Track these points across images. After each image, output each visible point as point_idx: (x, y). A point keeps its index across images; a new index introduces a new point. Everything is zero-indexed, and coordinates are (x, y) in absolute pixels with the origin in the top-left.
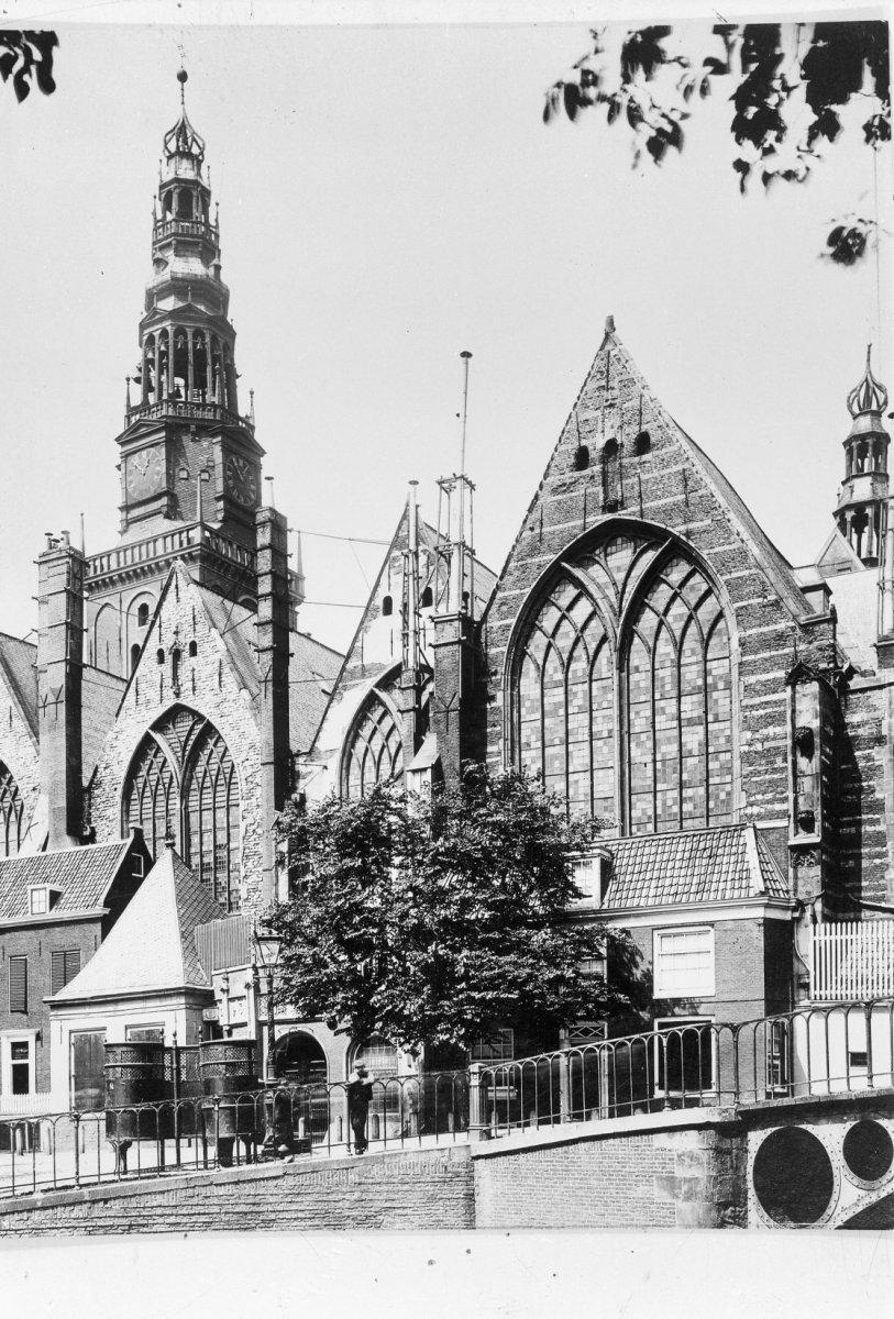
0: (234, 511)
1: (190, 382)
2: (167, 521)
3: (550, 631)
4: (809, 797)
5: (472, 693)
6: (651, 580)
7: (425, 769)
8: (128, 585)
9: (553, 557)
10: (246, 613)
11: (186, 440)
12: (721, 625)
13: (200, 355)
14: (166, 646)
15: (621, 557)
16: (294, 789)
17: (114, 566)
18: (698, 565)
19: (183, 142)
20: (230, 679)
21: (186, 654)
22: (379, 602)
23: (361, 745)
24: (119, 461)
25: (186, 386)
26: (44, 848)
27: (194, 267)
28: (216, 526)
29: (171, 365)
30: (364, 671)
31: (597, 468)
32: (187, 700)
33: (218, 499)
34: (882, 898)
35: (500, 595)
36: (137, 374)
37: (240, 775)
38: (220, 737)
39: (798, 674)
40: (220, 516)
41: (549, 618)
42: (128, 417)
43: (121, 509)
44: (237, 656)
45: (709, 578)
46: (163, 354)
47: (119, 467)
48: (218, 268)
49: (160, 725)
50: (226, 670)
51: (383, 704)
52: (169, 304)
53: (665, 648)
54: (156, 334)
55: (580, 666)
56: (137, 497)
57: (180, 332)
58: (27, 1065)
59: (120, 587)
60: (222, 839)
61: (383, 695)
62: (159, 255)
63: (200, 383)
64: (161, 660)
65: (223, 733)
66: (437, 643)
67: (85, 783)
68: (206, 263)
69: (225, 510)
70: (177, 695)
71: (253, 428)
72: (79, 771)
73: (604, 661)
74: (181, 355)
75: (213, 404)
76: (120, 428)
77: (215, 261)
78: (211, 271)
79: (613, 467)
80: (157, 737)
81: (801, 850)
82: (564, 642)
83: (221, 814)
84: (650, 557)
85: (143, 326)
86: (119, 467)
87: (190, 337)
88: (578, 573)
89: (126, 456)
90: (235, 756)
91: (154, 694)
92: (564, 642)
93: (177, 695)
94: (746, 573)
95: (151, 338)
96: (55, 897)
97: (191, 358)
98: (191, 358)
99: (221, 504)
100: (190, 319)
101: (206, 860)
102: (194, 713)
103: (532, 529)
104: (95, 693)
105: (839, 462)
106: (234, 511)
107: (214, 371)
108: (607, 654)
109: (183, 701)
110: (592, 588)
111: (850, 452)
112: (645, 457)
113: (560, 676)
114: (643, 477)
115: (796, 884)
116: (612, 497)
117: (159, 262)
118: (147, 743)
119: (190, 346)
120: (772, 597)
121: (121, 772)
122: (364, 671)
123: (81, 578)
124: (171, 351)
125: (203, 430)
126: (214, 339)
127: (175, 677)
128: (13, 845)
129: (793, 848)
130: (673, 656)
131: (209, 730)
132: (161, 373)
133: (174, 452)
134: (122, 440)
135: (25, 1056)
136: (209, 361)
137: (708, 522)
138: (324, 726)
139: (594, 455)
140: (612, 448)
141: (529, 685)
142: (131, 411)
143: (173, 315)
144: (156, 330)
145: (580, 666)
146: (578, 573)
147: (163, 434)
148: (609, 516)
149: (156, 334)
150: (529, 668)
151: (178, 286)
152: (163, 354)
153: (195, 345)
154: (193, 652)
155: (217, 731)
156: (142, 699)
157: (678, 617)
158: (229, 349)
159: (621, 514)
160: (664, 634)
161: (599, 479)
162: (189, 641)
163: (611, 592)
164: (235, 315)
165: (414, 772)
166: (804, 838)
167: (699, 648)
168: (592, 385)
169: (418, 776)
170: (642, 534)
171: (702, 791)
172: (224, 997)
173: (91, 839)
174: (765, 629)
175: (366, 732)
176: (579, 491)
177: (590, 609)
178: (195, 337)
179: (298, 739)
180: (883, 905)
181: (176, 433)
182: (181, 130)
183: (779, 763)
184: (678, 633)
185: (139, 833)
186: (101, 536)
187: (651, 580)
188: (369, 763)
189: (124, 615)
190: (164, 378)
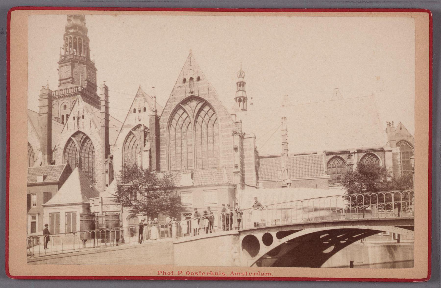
0: (89, 84)
1: (78, 50)
2: (71, 85)
3: (177, 120)
5: (155, 134)
6: (200, 110)
7: (147, 151)
8: (60, 100)
10: (97, 110)
11: (76, 64)
12: (216, 121)
13: (80, 45)
14: (76, 116)
15: (193, 104)
16: (110, 154)
18: (211, 108)
21: (81, 118)
22: (132, 110)
23: (127, 144)
24: (58, 68)
25: (76, 51)
26: (41, 165)
28: (85, 87)
29: (73, 46)
30: (127, 126)
33: (85, 80)
35: (165, 111)
36: (62, 47)
37: (96, 149)
38: (90, 140)
39: (235, 133)
40: (86, 85)
41: (177, 117)
42: (61, 57)
43: (59, 80)
45: (214, 111)
46: (70, 43)
47: (58, 70)
48: (85, 23)
49: (74, 135)
50: (92, 123)
51: (133, 134)
53: (204, 125)
54: (69, 38)
55: (184, 129)
56: (63, 78)
57: (75, 38)
58: (35, 222)
59: (58, 100)
60: (90, 165)
61: (133, 132)
62: (69, 18)
63: (80, 51)
65: (91, 139)
66: (146, 121)
67: (53, 149)
68: (82, 22)
69: (87, 83)
70: (79, 128)
71: (94, 64)
72: (51, 146)
73: (190, 128)
74: (75, 44)
75: (84, 57)
77: (84, 22)
78: (83, 24)
80: (73, 138)
82: (180, 123)
83: (90, 159)
84: (201, 104)
85: (65, 35)
86: (58, 70)
87: (78, 40)
88: (183, 106)
89: (60, 67)
90: (95, 144)
91: (72, 127)
92: (180, 123)
93: (79, 128)
95: (67, 39)
96: (45, 177)
97: (78, 45)
98: (78, 45)
99: (86, 82)
100: (78, 35)
101: (86, 170)
102: (83, 133)
104: (55, 125)
105: (235, 87)
106: (89, 84)
107: (84, 49)
108: (191, 125)
109: (80, 130)
110: (187, 111)
111: (238, 85)
112: (199, 82)
113: (180, 131)
114: (199, 86)
116: (192, 90)
118: (70, 139)
119: (78, 41)
121: (63, 147)
122: (127, 126)
123: (50, 98)
124: (73, 43)
125: (81, 62)
126: (84, 41)
127: (78, 124)
128: (31, 164)
129: (234, 172)
130: (206, 128)
131: (87, 137)
132: (70, 47)
133: (73, 67)
134: (59, 63)
135: (35, 219)
136: (83, 46)
138: (117, 139)
140: (191, 79)
141: (172, 133)
142: (62, 56)
143: (73, 33)
145: (184, 129)
146: (183, 106)
148: (191, 95)
149: (69, 38)
150: (172, 129)
151: (74, 27)
152: (70, 43)
153: (79, 42)
155: (89, 138)
156: (69, 129)
157: (207, 119)
158: (88, 44)
159: (193, 94)
160: (204, 123)
161: (188, 86)
162: (82, 115)
163: (191, 112)
164: (89, 35)
165: (144, 151)
166: (236, 170)
167: (212, 126)
169: (145, 152)
170: (199, 99)
171: (213, 159)
172: (93, 205)
173: (54, 163)
175: (129, 140)
176: (184, 88)
177: (187, 116)
178: (79, 40)
179: (111, 142)
181: (74, 62)
183: (230, 153)
184: (207, 122)
185: (68, 161)
186: (54, 87)
187: (200, 110)
188: (130, 148)
189: (60, 106)
190: (71, 49)
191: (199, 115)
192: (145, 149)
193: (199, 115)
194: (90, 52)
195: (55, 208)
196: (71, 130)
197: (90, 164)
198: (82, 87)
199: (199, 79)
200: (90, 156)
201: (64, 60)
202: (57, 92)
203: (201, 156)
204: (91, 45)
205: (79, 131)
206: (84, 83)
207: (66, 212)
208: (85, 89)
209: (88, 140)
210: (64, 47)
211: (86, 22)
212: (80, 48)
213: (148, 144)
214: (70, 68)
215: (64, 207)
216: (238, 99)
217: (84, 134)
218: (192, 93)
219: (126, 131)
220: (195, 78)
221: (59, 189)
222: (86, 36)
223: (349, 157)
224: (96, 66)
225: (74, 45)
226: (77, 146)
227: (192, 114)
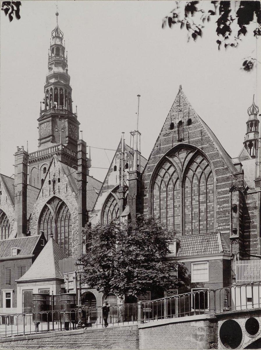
2: (52, 143)
3: (162, 176)
4: (236, 224)
7: (126, 216)
9: (163, 155)
11: (57, 120)
12: (211, 175)
13: (62, 95)
15: (183, 155)
17: (50, 152)
18: (205, 157)
19: (57, 34)
20: (69, 189)
21: (57, 182)
22: (113, 167)
23: (107, 209)
24: (38, 126)
27: (60, 70)
28: (66, 145)
30: (108, 187)
31: (176, 129)
32: (57, 195)
33: (66, 137)
34: (256, 253)
35: (148, 165)
36: (43, 101)
37: (72, 217)
39: (233, 189)
40: (67, 142)
41: (162, 172)
42: (41, 113)
43: (38, 140)
44: (71, 183)
45: (208, 161)
46: (51, 95)
48: (67, 70)
49: (49, 202)
50: (68, 186)
51: (114, 197)
52: (53, 81)
53: (195, 181)
55: (171, 186)
57: (56, 89)
59: (38, 162)
60: (67, 235)
61: (114, 194)
62: (50, 66)
63: (62, 104)
64: (50, 183)
67: (28, 219)
69: (69, 140)
70: (54, 193)
74: (56, 95)
75: (65, 110)
76: (38, 116)
77: (66, 68)
78: (65, 71)
79: (181, 129)
80: (48, 205)
81: (233, 239)
82: (166, 179)
83: (67, 228)
84: (191, 155)
86: (38, 128)
87: (59, 90)
89: (40, 125)
92: (166, 179)
93: (54, 193)
94: (218, 160)
96: (19, 251)
99: (67, 139)
100: (59, 85)
102: (59, 199)
103: (157, 146)
110: (174, 164)
111: (248, 125)
112: (190, 126)
113: (165, 189)
114: (190, 132)
115: (232, 249)
116: (180, 137)
117: (50, 69)
118: (46, 207)
119: (64, 93)
120: (226, 167)
121: (38, 215)
122: (108, 187)
123: (27, 160)
124: (53, 94)
125: (62, 117)
126: (66, 91)
127: (54, 188)
128: (7, 236)
129: (231, 239)
131: (63, 203)
132: (50, 101)
136: (64, 97)
137: (208, 145)
139: (175, 125)
140: (181, 123)
142: (42, 111)
143: (54, 84)
144: (49, 88)
145: (171, 186)
146: (171, 159)
147: (51, 118)
148: (180, 143)
150: (156, 187)
151: (55, 75)
152: (51, 95)
153: (60, 92)
154: (59, 181)
156: (44, 194)
158: (70, 93)
159: (183, 143)
160: (195, 177)
161: (177, 132)
162: (58, 178)
165: (123, 216)
167: (205, 182)
168: (175, 105)
170: (189, 148)
171: (205, 222)
172: (67, 281)
174: (224, 176)
175: (109, 205)
177: (174, 170)
178: (60, 90)
179: (89, 207)
180: (256, 255)
182: (57, 30)
184: (199, 177)
188: (110, 214)
190: (51, 102)
191: (189, 169)
192: (123, 214)
193: (189, 169)
194: (73, 103)
195: (28, 284)
196: (46, 195)
197: (66, 235)
198: (63, 145)
199: (190, 122)
200: (67, 223)
201: (44, 116)
202: (36, 154)
203: (191, 220)
204: (74, 96)
205: (54, 196)
206: (65, 140)
207: (39, 289)
208: (65, 147)
209: (64, 207)
210: (45, 101)
211: (69, 68)
212: (62, 99)
213: (127, 208)
214: (50, 124)
215: (37, 283)
216: (248, 143)
217: (60, 200)
218: (180, 140)
219: (105, 195)
220: (185, 121)
221: (33, 263)
222: (68, 85)
223: (83, 231)
224: (79, 119)
225: (55, 98)
226: (53, 214)
227: (181, 167)
